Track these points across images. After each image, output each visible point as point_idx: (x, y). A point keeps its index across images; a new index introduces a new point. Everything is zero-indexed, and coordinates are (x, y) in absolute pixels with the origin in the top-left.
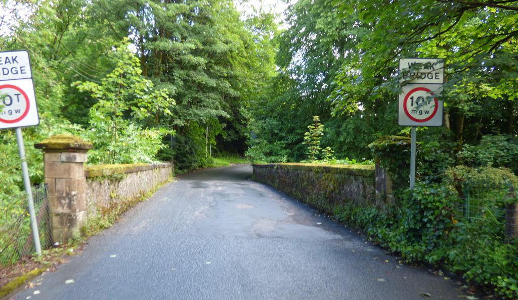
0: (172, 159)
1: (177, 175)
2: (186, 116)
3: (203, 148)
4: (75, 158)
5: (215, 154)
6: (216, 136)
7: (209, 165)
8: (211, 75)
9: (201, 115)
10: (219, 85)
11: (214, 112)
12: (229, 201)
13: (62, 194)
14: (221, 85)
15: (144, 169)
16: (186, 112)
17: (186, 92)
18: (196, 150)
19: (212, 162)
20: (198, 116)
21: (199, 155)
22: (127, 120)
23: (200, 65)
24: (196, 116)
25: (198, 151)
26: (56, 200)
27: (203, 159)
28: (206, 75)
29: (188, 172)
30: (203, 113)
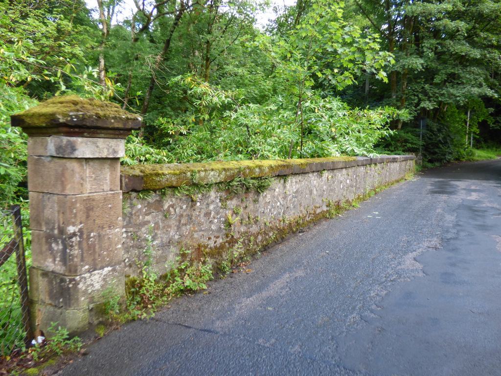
0: (421, 150)
1: (424, 171)
2: (437, 97)
3: (462, 137)
4: (74, 149)
5: (478, 144)
6: (479, 123)
7: (470, 157)
8: (473, 44)
9: (458, 94)
10: (485, 57)
11: (476, 90)
12: (484, 228)
13: (53, 229)
14: (488, 55)
15: (340, 166)
16: (437, 91)
17: (439, 67)
18: (452, 140)
19: (473, 154)
20: (453, 97)
21: (455, 146)
22: (318, 90)
23: (458, 31)
24: (451, 97)
25: (454, 140)
26: (44, 240)
27: (462, 151)
28: (468, 45)
29: (441, 166)
30: (458, 93)
